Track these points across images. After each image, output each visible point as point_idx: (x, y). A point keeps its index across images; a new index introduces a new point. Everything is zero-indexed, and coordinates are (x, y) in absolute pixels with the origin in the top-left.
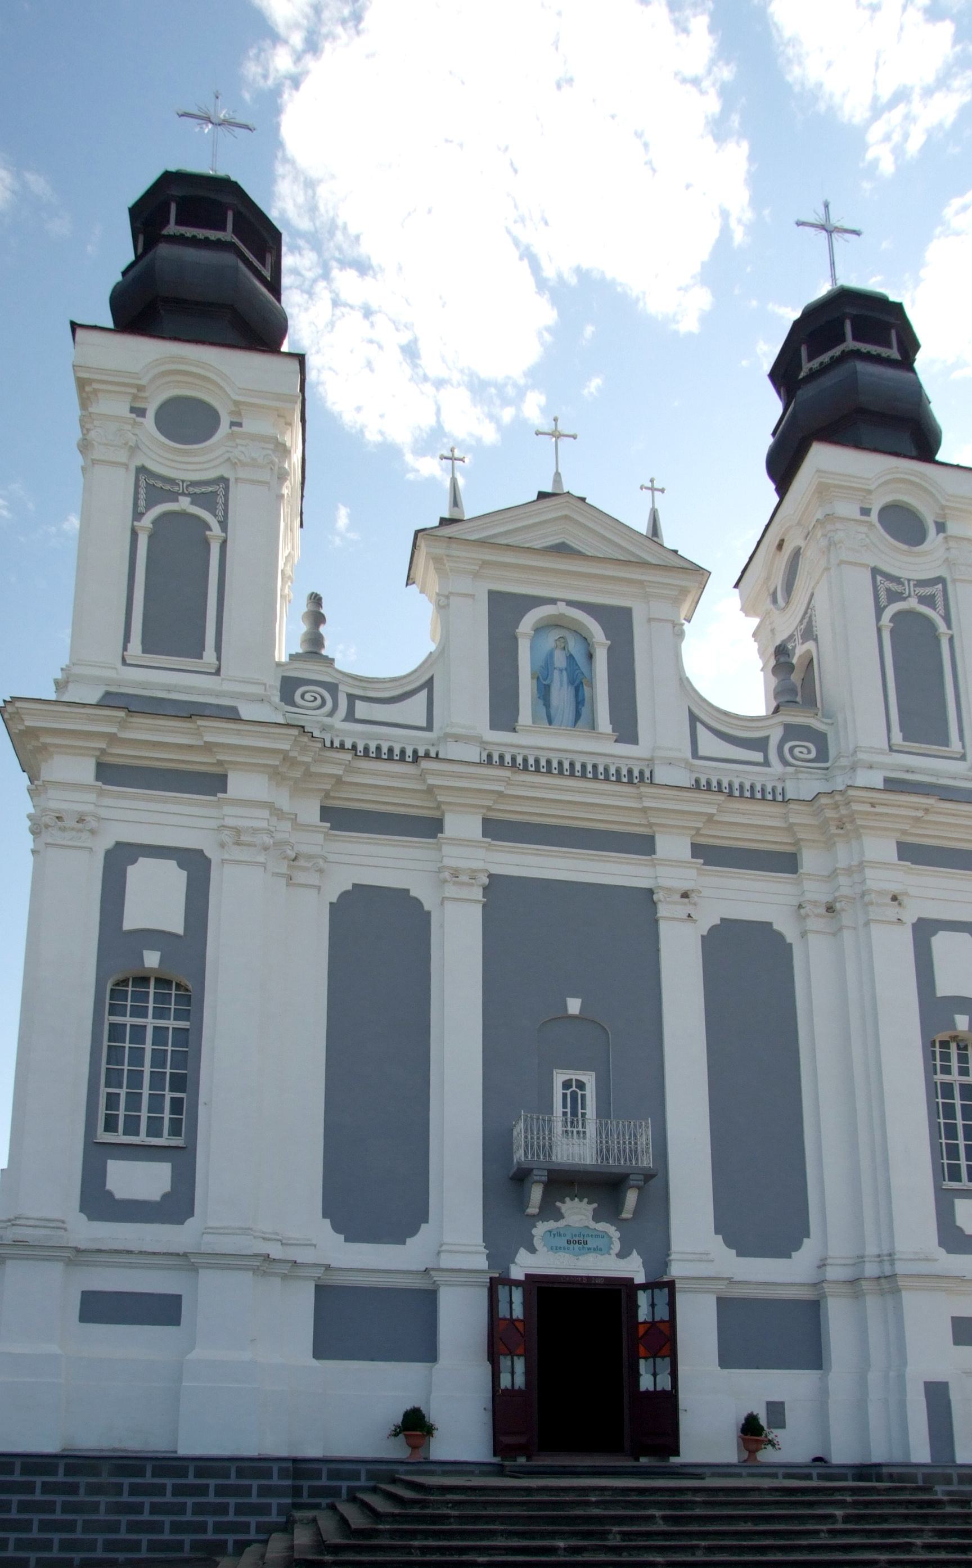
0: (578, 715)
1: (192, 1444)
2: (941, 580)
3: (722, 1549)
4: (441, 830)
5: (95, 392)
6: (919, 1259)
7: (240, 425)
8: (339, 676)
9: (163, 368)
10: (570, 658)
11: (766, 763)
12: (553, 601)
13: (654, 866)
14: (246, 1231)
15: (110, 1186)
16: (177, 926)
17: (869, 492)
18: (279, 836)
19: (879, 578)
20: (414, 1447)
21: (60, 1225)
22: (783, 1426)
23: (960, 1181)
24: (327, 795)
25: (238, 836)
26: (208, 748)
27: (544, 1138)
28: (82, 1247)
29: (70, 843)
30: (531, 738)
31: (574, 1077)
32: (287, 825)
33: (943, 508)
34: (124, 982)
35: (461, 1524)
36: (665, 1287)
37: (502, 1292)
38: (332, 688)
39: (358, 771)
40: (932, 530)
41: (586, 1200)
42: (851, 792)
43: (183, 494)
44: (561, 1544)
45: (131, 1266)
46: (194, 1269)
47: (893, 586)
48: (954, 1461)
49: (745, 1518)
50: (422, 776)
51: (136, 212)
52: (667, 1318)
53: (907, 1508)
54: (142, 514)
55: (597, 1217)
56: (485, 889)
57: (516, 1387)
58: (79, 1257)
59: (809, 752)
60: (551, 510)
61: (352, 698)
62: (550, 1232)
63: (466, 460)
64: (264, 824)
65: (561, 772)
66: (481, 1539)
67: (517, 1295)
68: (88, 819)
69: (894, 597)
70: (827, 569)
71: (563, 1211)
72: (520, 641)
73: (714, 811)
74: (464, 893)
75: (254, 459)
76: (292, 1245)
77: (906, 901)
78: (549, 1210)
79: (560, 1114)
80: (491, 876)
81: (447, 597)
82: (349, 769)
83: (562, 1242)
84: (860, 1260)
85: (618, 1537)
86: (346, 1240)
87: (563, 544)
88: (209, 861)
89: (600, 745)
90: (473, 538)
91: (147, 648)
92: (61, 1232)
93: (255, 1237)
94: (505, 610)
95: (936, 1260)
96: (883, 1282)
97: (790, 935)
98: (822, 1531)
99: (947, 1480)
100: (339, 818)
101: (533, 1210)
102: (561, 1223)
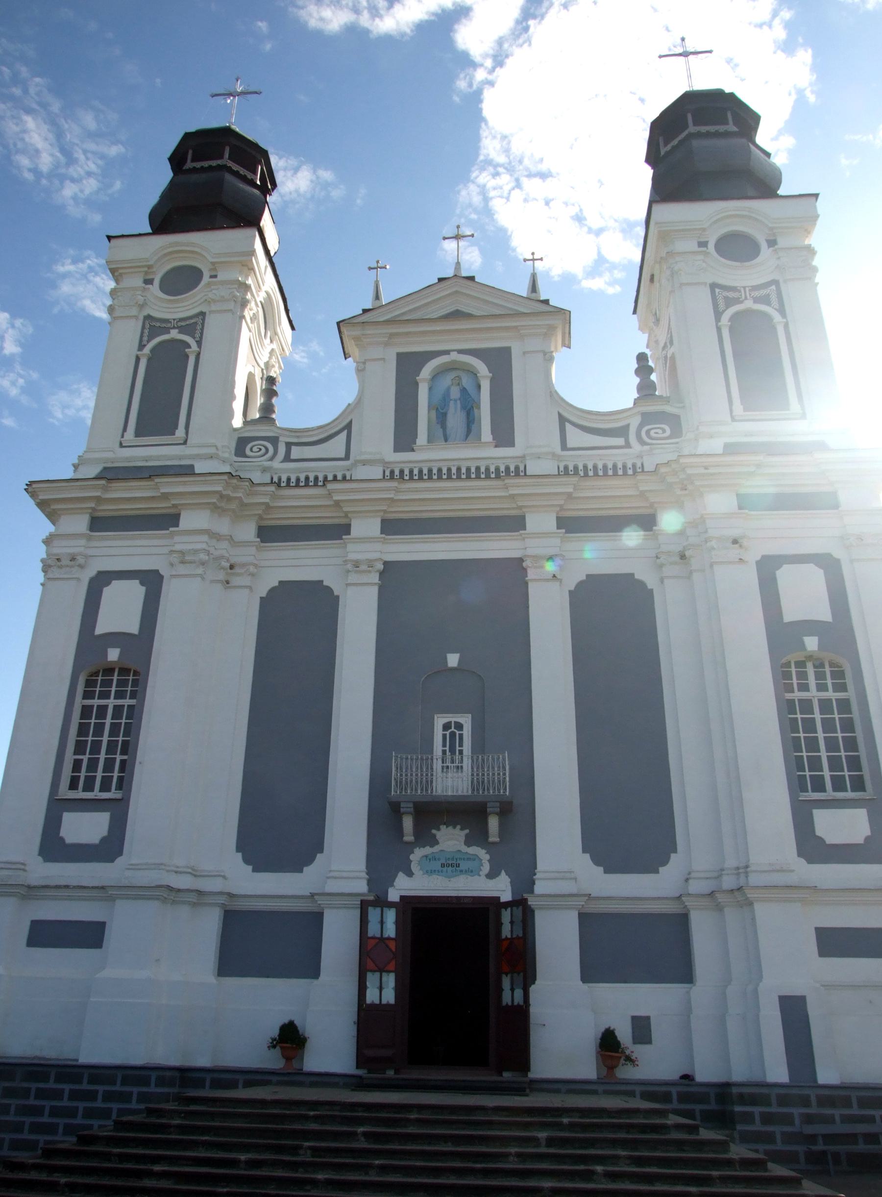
0: (469, 431)
1: (92, 1054)
2: (775, 282)
3: (395, 1169)
4: (348, 532)
5: (121, 275)
6: (773, 871)
7: (215, 276)
8: (280, 431)
9: (166, 251)
10: (464, 390)
11: (628, 445)
12: (447, 352)
13: (524, 539)
14: (158, 866)
15: (62, 833)
16: (133, 627)
17: (704, 230)
18: (217, 553)
19: (717, 290)
20: (288, 1059)
21: (23, 867)
22: (649, 1041)
23: (825, 791)
24: (261, 518)
25: (183, 558)
26: (165, 496)
27: (412, 775)
28: (34, 883)
29: (65, 576)
30: (427, 453)
31: (453, 720)
32: (225, 545)
33: (771, 229)
34: (96, 674)
35: (179, 1135)
36: (522, 907)
37: (374, 914)
38: (274, 441)
39: (282, 498)
40: (764, 245)
41: (459, 827)
42: (682, 460)
43: (174, 328)
44: (243, 1157)
45: (70, 898)
46: (112, 899)
47: (731, 295)
48: (815, 1080)
49: (445, 1138)
50: (330, 495)
51: (171, 159)
52: (521, 935)
53: (628, 1132)
54: (145, 346)
55: (468, 842)
56: (382, 574)
57: (516, 1003)
58: (32, 892)
59: (664, 431)
60: (446, 289)
61: (289, 445)
62: (426, 856)
63: (388, 267)
64: (204, 546)
65: (440, 477)
66: (585, 1148)
67: (391, 916)
68: (78, 558)
69: (729, 302)
70: (672, 292)
71: (437, 837)
72: (420, 385)
73: (571, 490)
74: (365, 579)
75: (223, 297)
76: (203, 876)
77: (745, 543)
78: (424, 837)
79: (440, 753)
80: (386, 563)
81: (364, 363)
82: (273, 496)
83: (437, 865)
84: (720, 873)
85: (309, 1152)
86: (254, 870)
87: (457, 311)
88: (162, 577)
89: (485, 452)
90: (382, 319)
91: (138, 433)
92: (21, 873)
93: (168, 871)
94: (408, 366)
95: (792, 871)
96: (736, 894)
97: (651, 582)
98: (510, 1154)
99: (805, 1101)
100: (268, 534)
101: (409, 837)
102: (436, 849)
